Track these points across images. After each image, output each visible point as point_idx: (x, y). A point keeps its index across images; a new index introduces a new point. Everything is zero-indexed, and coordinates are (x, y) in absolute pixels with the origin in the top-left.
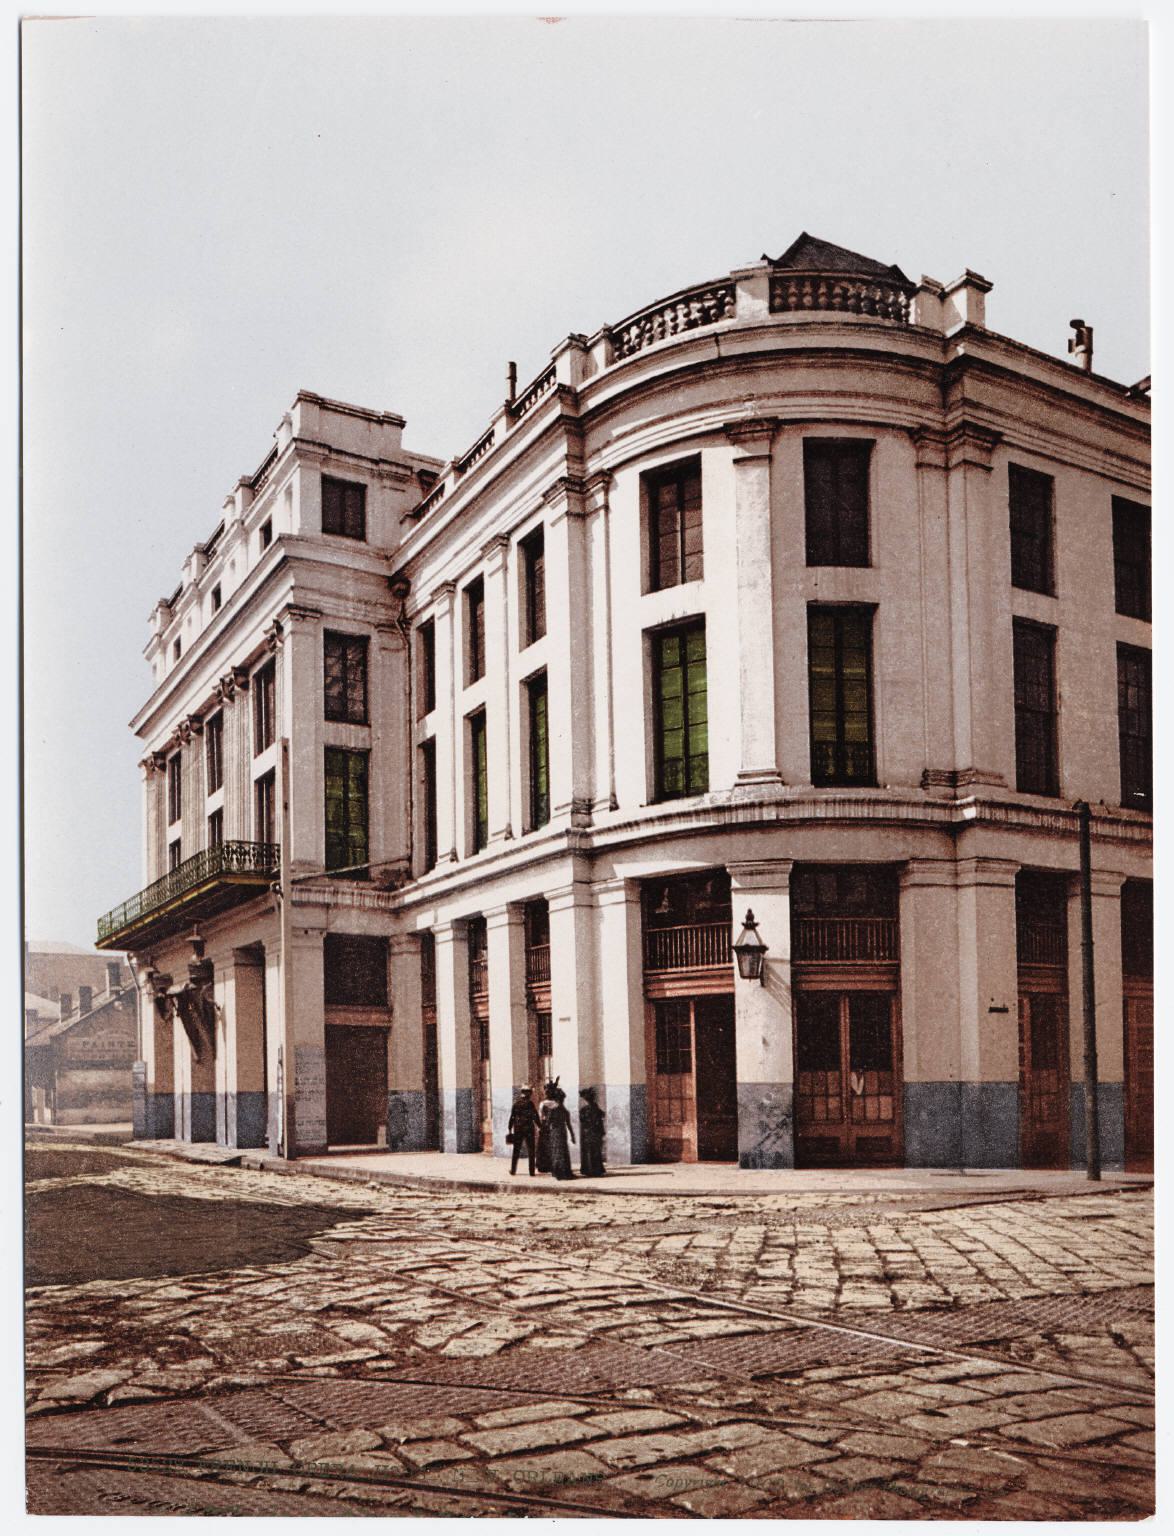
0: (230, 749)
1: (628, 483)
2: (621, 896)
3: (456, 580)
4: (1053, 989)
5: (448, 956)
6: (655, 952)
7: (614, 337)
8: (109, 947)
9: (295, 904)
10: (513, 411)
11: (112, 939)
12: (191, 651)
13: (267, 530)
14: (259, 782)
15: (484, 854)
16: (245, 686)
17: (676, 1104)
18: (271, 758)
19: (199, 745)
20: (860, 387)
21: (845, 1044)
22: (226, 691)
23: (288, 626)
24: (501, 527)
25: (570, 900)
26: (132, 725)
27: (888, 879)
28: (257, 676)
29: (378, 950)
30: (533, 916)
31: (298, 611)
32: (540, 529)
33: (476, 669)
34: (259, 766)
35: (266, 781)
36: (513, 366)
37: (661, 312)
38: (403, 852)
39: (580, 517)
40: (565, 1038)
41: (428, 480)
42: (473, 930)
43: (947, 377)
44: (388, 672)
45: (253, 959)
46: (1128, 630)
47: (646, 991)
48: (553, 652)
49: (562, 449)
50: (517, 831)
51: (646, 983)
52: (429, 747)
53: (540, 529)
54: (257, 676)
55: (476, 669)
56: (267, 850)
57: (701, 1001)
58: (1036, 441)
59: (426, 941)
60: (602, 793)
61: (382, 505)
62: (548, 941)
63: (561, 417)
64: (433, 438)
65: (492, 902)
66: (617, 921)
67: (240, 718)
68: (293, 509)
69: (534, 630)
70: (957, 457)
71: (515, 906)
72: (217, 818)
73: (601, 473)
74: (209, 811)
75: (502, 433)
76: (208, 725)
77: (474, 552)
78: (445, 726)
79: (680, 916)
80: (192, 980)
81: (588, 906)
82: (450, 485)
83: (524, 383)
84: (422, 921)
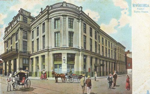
1: (53, 19)
2: (52, 55)
5: (40, 59)
7: (51, 6)
9: (20, 55)
10: (42, 12)
13: (17, 21)
14: (16, 44)
17: (26, 46)
18: (17, 41)
20: (95, 48)
22: (13, 35)
23: (19, 29)
27: (74, 55)
30: (43, 57)
31: (21, 29)
32: (45, 23)
33: (38, 34)
34: (16, 42)
35: (17, 44)
38: (30, 51)
39: (48, 21)
40: (46, 67)
42: (37, 58)
43: (79, 15)
46: (106, 47)
48: (45, 33)
49: (47, 15)
50: (42, 49)
53: (45, 23)
54: (16, 34)
55: (38, 34)
56: (17, 50)
58: (74, 10)
59: (32, 59)
60: (50, 46)
64: (34, 14)
66: (51, 57)
68: (21, 19)
69: (44, 31)
72: (11, 47)
75: (41, 14)
77: (38, 24)
82: (35, 18)
83: (43, 10)
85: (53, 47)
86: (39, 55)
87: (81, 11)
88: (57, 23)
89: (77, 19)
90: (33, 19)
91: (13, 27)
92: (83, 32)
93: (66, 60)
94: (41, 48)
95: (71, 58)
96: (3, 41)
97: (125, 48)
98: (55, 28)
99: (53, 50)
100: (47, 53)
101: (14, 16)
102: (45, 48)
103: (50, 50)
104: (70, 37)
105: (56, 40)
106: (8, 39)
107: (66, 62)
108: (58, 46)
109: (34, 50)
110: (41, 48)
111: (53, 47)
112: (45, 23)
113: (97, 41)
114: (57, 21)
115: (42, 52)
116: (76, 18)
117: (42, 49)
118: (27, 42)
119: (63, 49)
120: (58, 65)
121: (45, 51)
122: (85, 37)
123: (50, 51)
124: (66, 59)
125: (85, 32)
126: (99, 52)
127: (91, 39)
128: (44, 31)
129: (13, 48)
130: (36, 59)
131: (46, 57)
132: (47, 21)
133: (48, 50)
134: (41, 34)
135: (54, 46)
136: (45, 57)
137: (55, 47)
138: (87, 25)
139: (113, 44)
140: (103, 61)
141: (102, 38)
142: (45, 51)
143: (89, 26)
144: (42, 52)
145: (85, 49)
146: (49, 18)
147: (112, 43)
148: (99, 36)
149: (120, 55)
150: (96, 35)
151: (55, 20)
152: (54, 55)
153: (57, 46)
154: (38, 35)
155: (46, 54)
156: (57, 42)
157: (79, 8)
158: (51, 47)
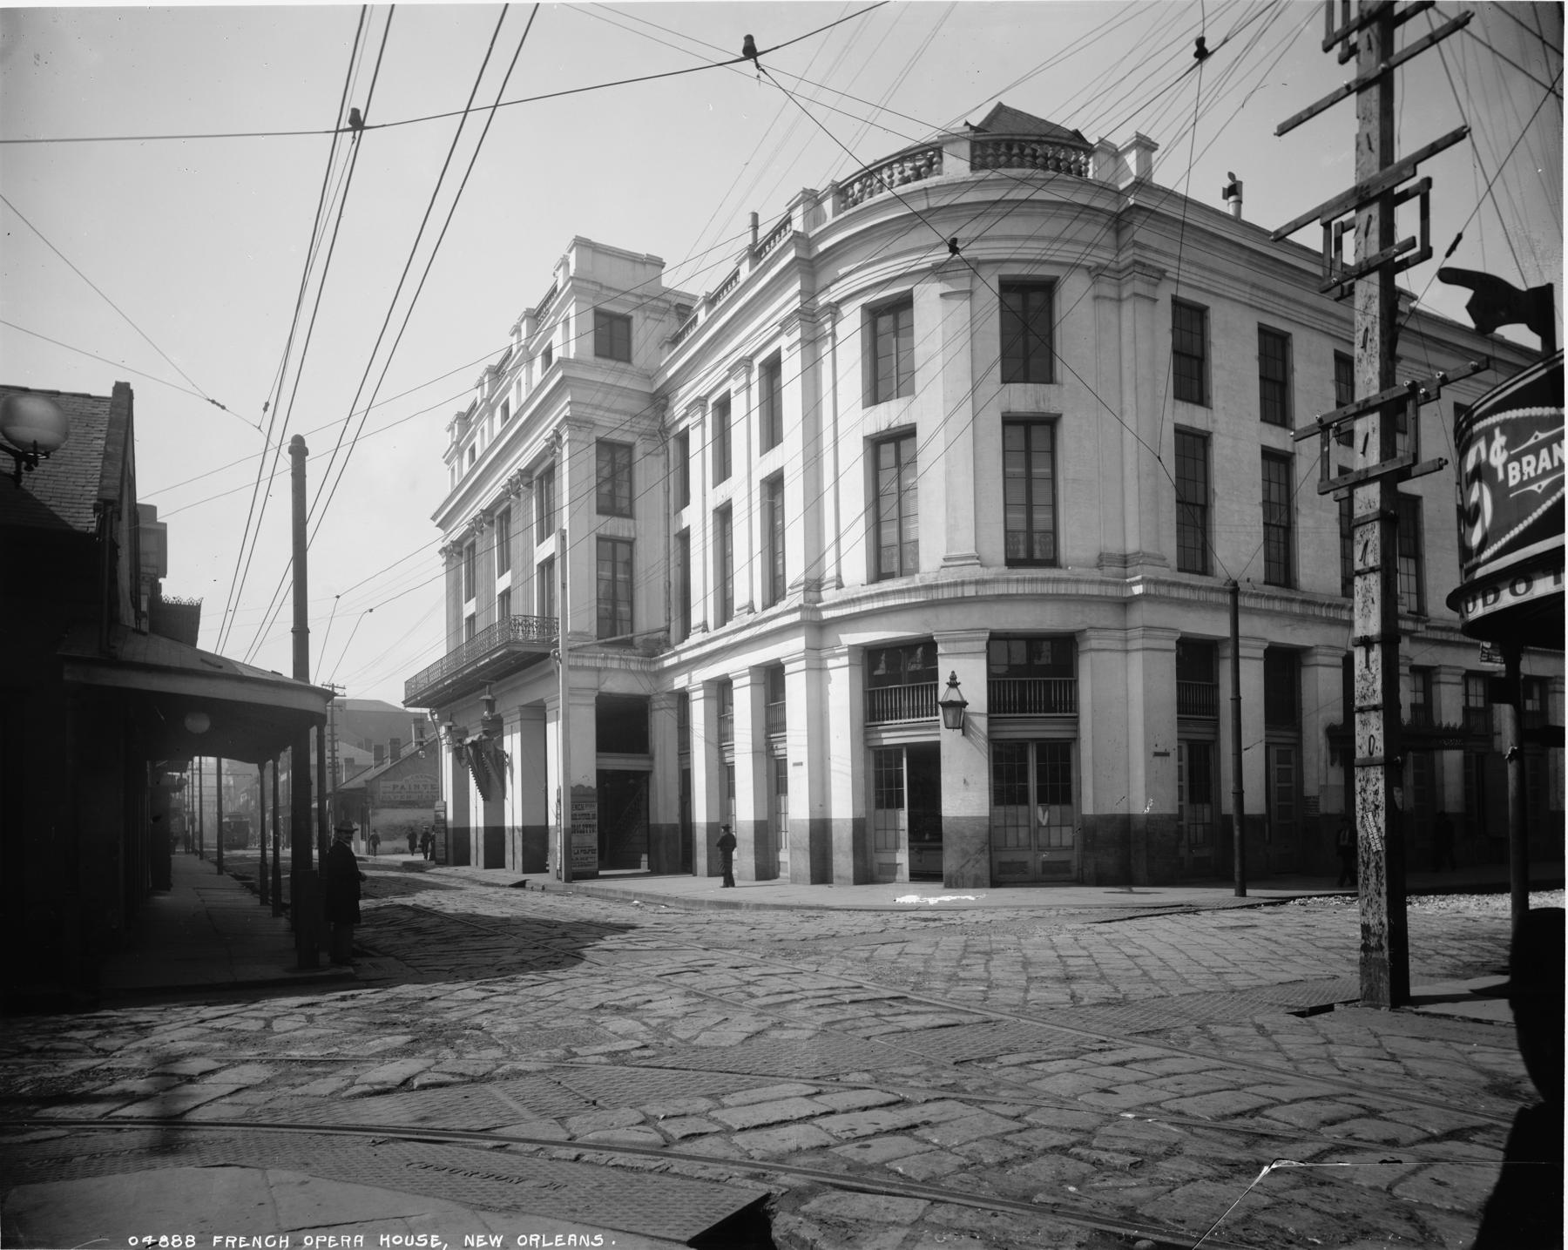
0: (516, 544)
5: (743, 701)
9: (571, 668)
12: (518, 415)
13: (548, 354)
14: (541, 566)
15: (730, 626)
16: (491, 523)
22: (513, 488)
24: (701, 391)
25: (802, 665)
26: (434, 518)
28: (541, 477)
30: (772, 678)
33: (723, 470)
36: (755, 216)
38: (662, 624)
41: (683, 310)
42: (721, 689)
44: (649, 473)
45: (536, 717)
47: (866, 740)
48: (789, 456)
50: (758, 606)
51: (866, 733)
52: (684, 537)
54: (541, 477)
59: (683, 697)
61: (645, 333)
64: (689, 277)
65: (737, 666)
66: (841, 686)
69: (772, 436)
71: (708, 684)
73: (829, 305)
74: (538, 559)
76: (498, 517)
77: (722, 372)
78: (697, 517)
79: (897, 675)
81: (817, 670)
83: (763, 232)
86: (737, 666)
89: (1096, 272)
91: (518, 415)
96: (438, 539)
100: (798, 643)
101: (794, 191)
102: (783, 597)
103: (826, 615)
104: (1020, 470)
106: (476, 526)
112: (784, 355)
114: (885, 323)
117: (758, 606)
118: (630, 543)
122: (1193, 448)
128: (772, 436)
129: (517, 608)
130: (761, 690)
131: (796, 687)
132: (797, 335)
134: (750, 464)
136: (736, 693)
141: (1264, 331)
143: (465, 606)
151: (873, 313)
158: (840, 586)
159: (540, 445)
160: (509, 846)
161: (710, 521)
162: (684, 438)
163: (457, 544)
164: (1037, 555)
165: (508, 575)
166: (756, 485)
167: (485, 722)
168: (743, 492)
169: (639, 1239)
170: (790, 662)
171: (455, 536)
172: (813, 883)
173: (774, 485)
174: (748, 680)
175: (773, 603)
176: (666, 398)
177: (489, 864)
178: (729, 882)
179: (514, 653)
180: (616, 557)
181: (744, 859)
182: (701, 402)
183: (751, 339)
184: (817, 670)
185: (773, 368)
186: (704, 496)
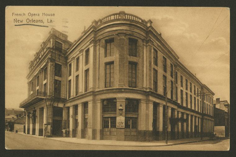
0: (40, 80)
3: (83, 50)
4: (137, 117)
6: (105, 109)
7: (100, 21)
8: (21, 107)
11: (22, 106)
14: (44, 85)
19: (42, 74)
20: (73, 69)
21: (110, 124)
24: (74, 56)
25: (92, 102)
27: (138, 101)
28: (45, 69)
29: (61, 109)
30: (85, 105)
33: (77, 69)
37: (105, 19)
42: (76, 107)
44: (64, 70)
45: (42, 110)
49: (93, 36)
52: (70, 81)
54: (45, 69)
57: (111, 118)
62: (88, 108)
63: (93, 31)
64: (72, 38)
66: (99, 105)
67: (42, 76)
69: (87, 62)
70: (148, 44)
71: (74, 106)
73: (99, 40)
74: (44, 84)
76: (37, 77)
77: (78, 52)
80: (107, 103)
84: (68, 105)
85: (102, 88)
87: (151, 26)
88: (108, 47)
90: (70, 44)
92: (152, 63)
93: (124, 111)
94: (81, 89)
95: (132, 106)
97: (213, 94)
98: (106, 56)
99: (101, 92)
105: (108, 76)
107: (124, 114)
108: (110, 87)
109: (72, 95)
110: (81, 89)
111: (102, 88)
113: (173, 80)
115: (83, 96)
116: (140, 38)
119: (120, 91)
120: (110, 119)
121: (88, 94)
122: (156, 72)
123: (98, 95)
124: (123, 107)
125: (156, 64)
126: (176, 99)
127: (165, 77)
131: (90, 105)
133: (94, 94)
134: (82, 67)
135: (104, 86)
137: (106, 87)
138: (159, 52)
139: (193, 85)
140: (188, 115)
142: (88, 94)
144: (83, 96)
145: (156, 91)
146: (97, 39)
147: (191, 84)
148: (177, 72)
149: (208, 106)
150: (172, 69)
152: (103, 101)
153: (108, 85)
154: (71, 75)
155: (89, 99)
156: (108, 80)
157: (147, 23)
159: (45, 64)
160: (36, 131)
161: (75, 78)
162: (70, 65)
163: (30, 82)
164: (133, 86)
165: (38, 87)
166: (84, 72)
167: (33, 111)
168: (81, 73)
169: (36, 26)
170: (90, 101)
171: (30, 80)
172: (100, 140)
173: (87, 71)
174: (81, 105)
175: (86, 91)
176: (67, 58)
177: (28, 134)
178: (25, 134)
179: (38, 98)
180: (57, 86)
181: (31, 132)
182: (74, 58)
183: (83, 47)
184: (94, 101)
185: (88, 51)
186: (74, 73)
